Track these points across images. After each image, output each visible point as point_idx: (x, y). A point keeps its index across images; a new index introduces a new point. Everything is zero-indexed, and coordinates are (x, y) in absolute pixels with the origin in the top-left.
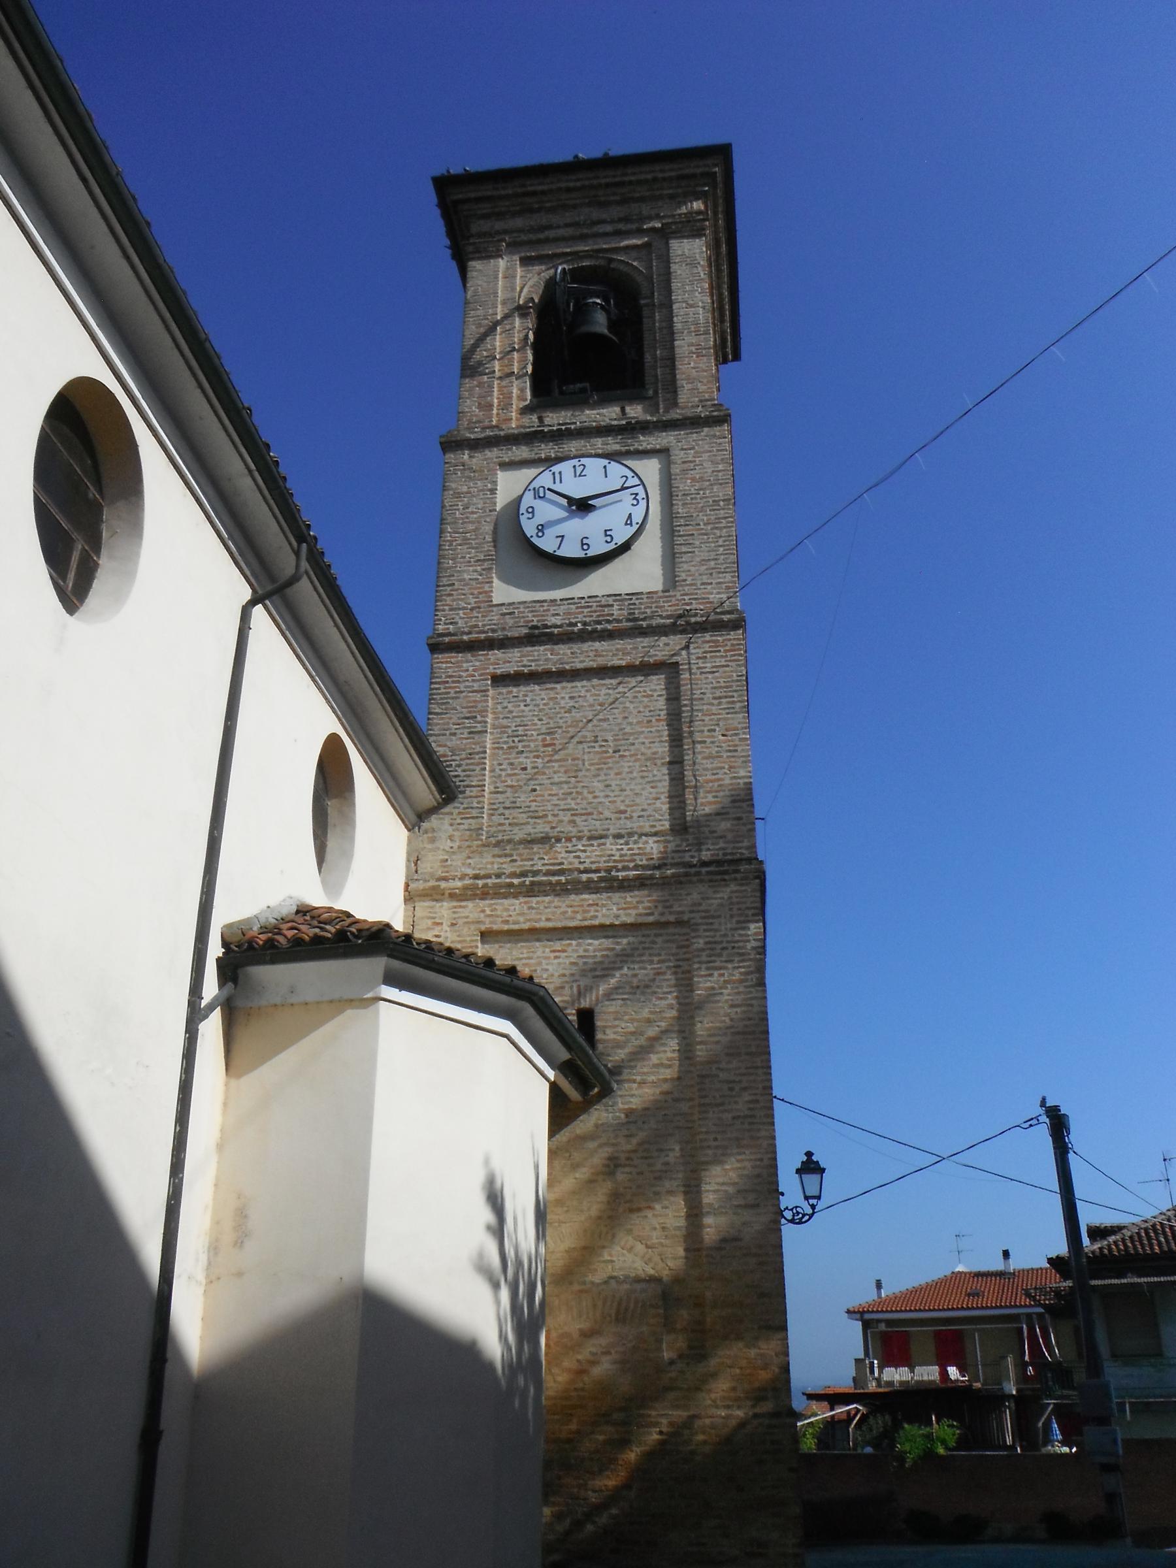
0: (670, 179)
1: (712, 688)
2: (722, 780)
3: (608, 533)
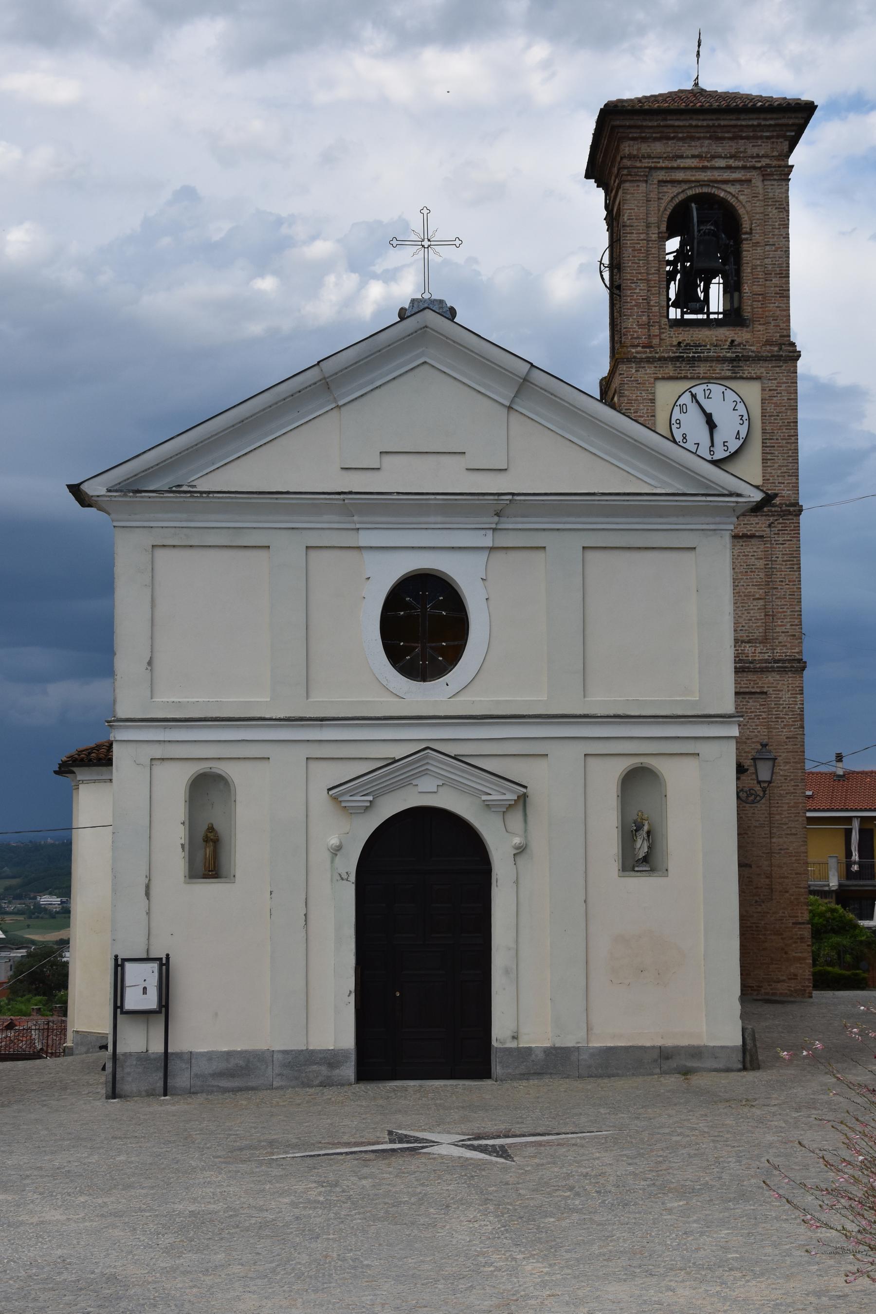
0: (770, 125)
1: (782, 554)
2: (786, 612)
3: (726, 444)
